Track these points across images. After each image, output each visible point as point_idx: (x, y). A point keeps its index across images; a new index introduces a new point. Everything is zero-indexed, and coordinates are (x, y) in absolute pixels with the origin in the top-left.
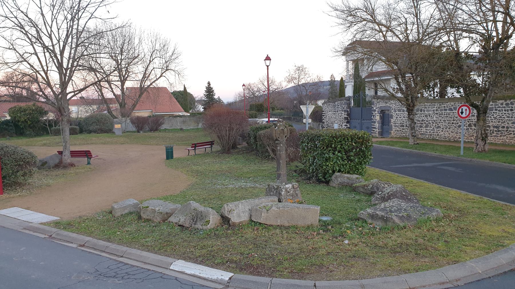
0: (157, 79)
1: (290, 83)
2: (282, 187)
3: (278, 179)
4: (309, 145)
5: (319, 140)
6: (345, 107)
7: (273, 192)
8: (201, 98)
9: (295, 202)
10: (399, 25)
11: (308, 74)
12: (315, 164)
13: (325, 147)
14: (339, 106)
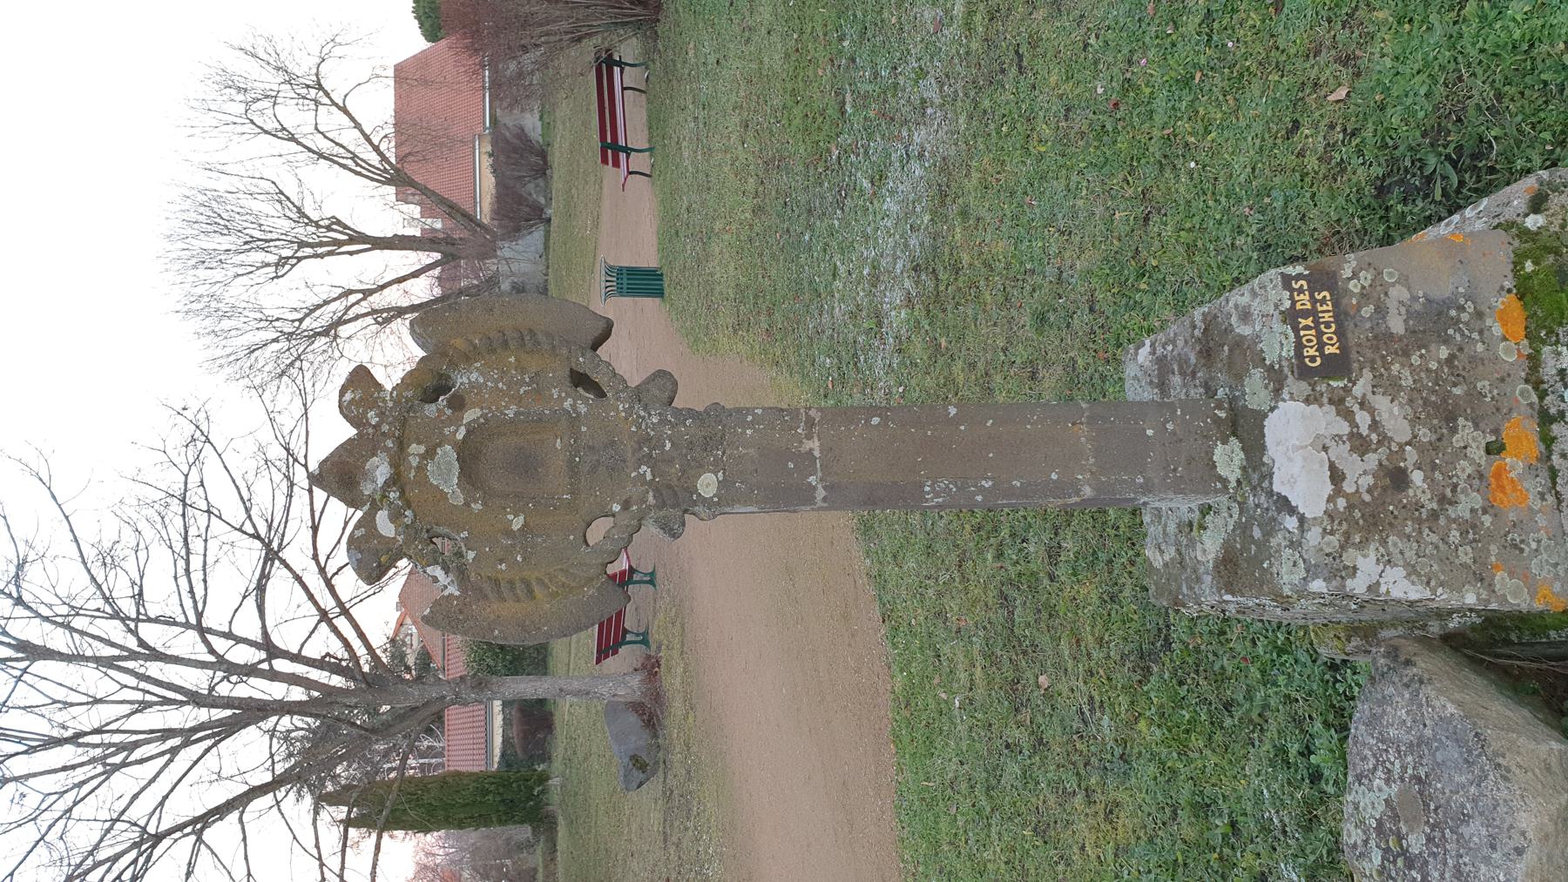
0: (358, 126)
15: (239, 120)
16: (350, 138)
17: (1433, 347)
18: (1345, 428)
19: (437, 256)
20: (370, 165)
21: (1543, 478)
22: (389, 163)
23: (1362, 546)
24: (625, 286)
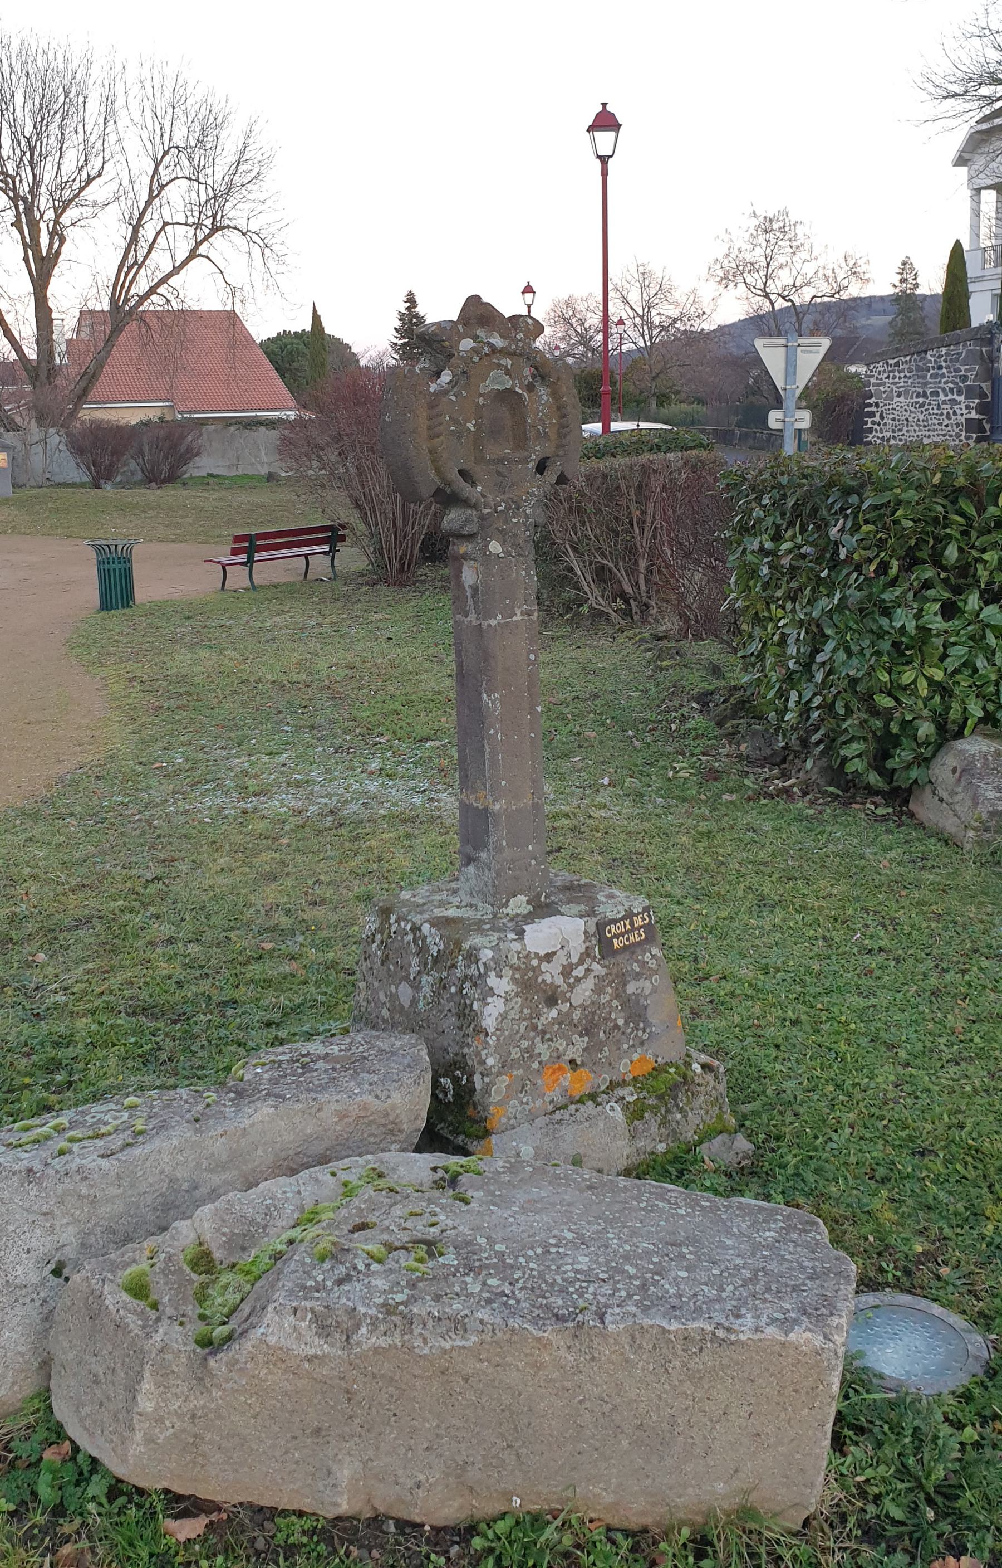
0: (176, 270)
1: (731, 285)
2: (486, 955)
3: (469, 860)
4: (787, 545)
5: (856, 514)
6: (971, 372)
7: (416, 986)
8: (380, 357)
9: (612, 1086)
10: (94, 1554)
11: (807, 247)
12: (819, 677)
13: (895, 564)
14: (940, 368)
15: (166, 137)
16: (161, 261)
17: (622, 1014)
18: (575, 960)
19: (32, 354)
20: (131, 283)
21: (561, 1101)
22: (140, 303)
23: (514, 980)
24: (112, 566)
